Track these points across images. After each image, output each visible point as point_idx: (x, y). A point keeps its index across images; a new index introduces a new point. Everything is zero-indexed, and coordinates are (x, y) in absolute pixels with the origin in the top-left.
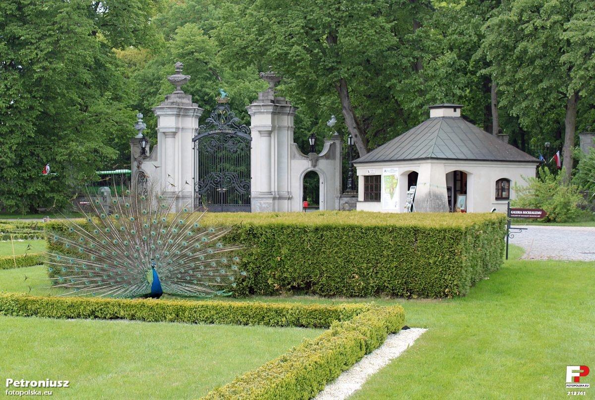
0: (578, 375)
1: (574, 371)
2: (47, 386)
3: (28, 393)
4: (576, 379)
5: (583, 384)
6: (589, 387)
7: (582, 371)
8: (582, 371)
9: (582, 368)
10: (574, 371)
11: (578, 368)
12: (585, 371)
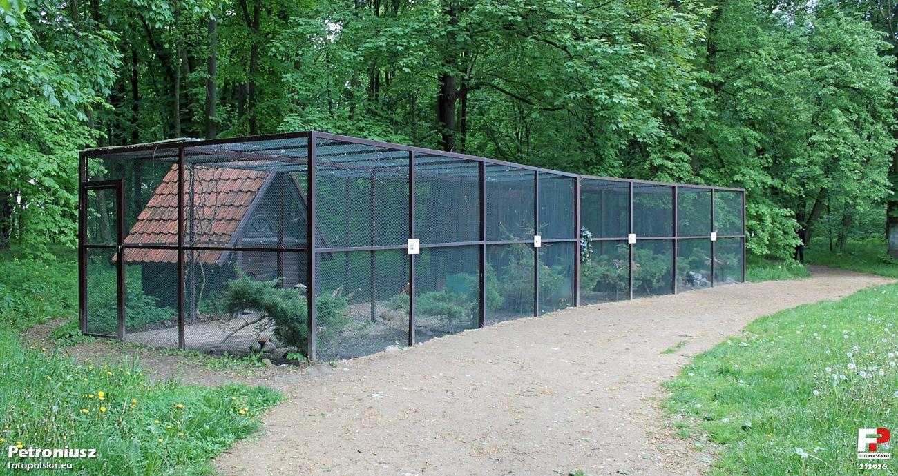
0: (874, 441)
1: (869, 436)
2: (66, 456)
3: (40, 466)
4: (872, 447)
5: (881, 454)
6: (889, 458)
7: (881, 436)
8: (881, 436)
9: (879, 431)
10: (869, 436)
11: (874, 431)
12: (884, 435)
